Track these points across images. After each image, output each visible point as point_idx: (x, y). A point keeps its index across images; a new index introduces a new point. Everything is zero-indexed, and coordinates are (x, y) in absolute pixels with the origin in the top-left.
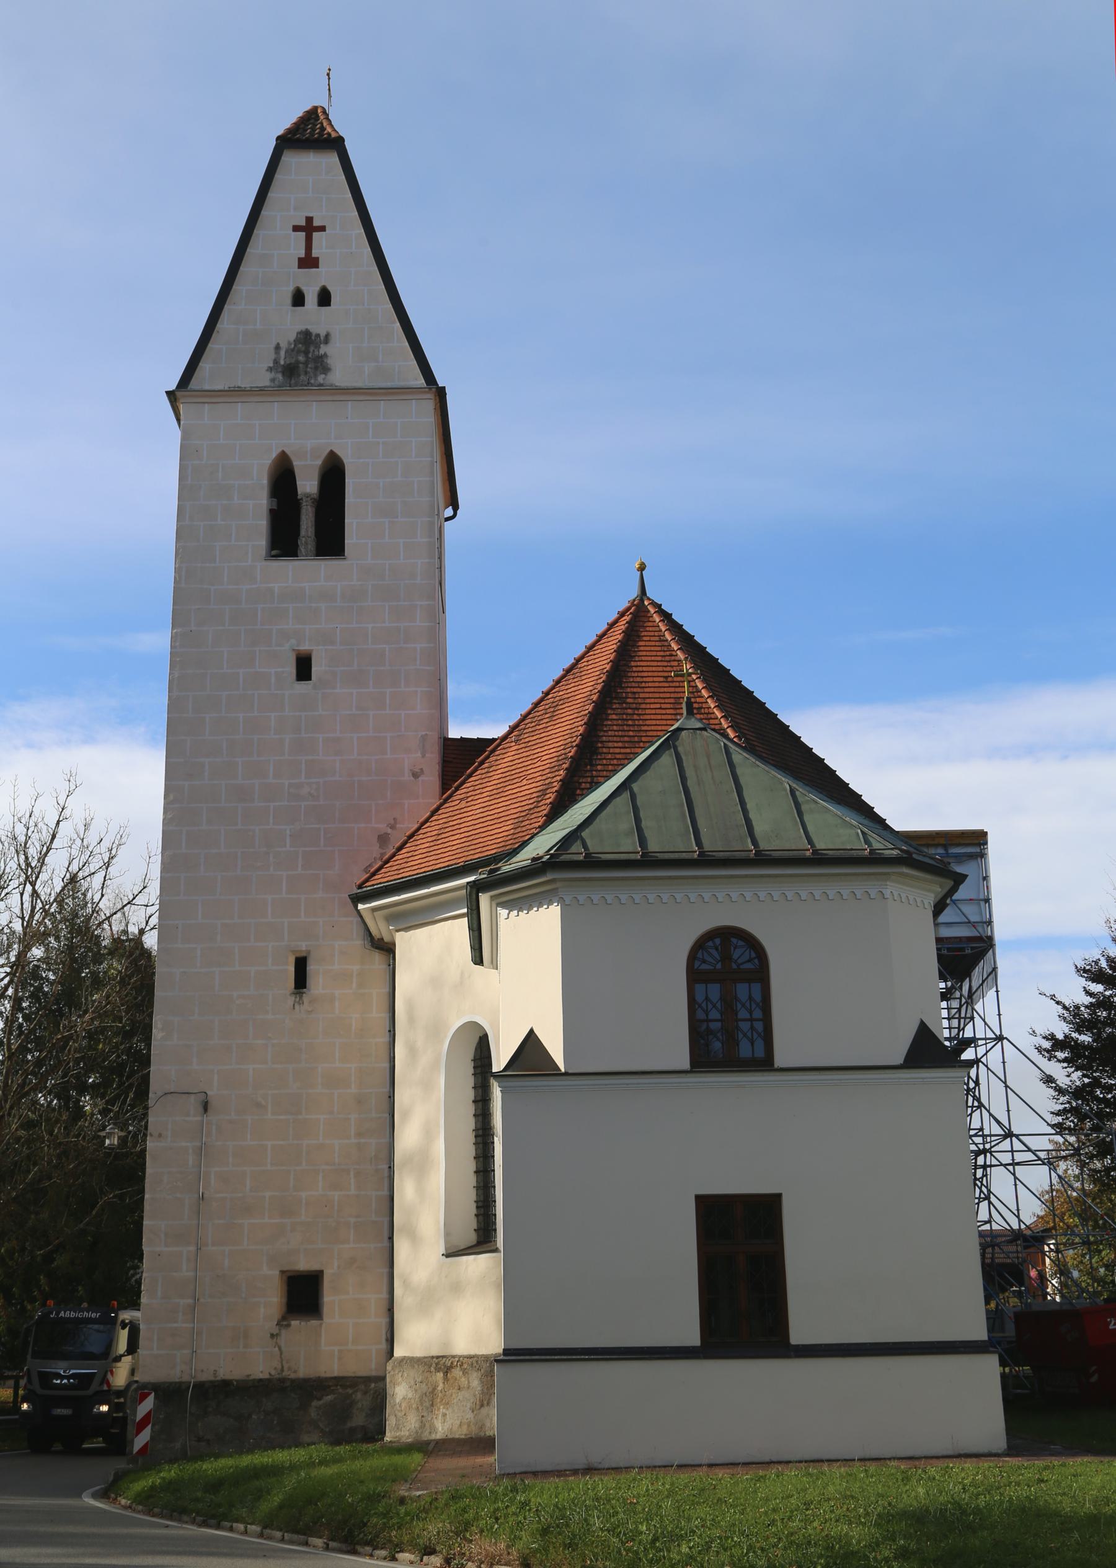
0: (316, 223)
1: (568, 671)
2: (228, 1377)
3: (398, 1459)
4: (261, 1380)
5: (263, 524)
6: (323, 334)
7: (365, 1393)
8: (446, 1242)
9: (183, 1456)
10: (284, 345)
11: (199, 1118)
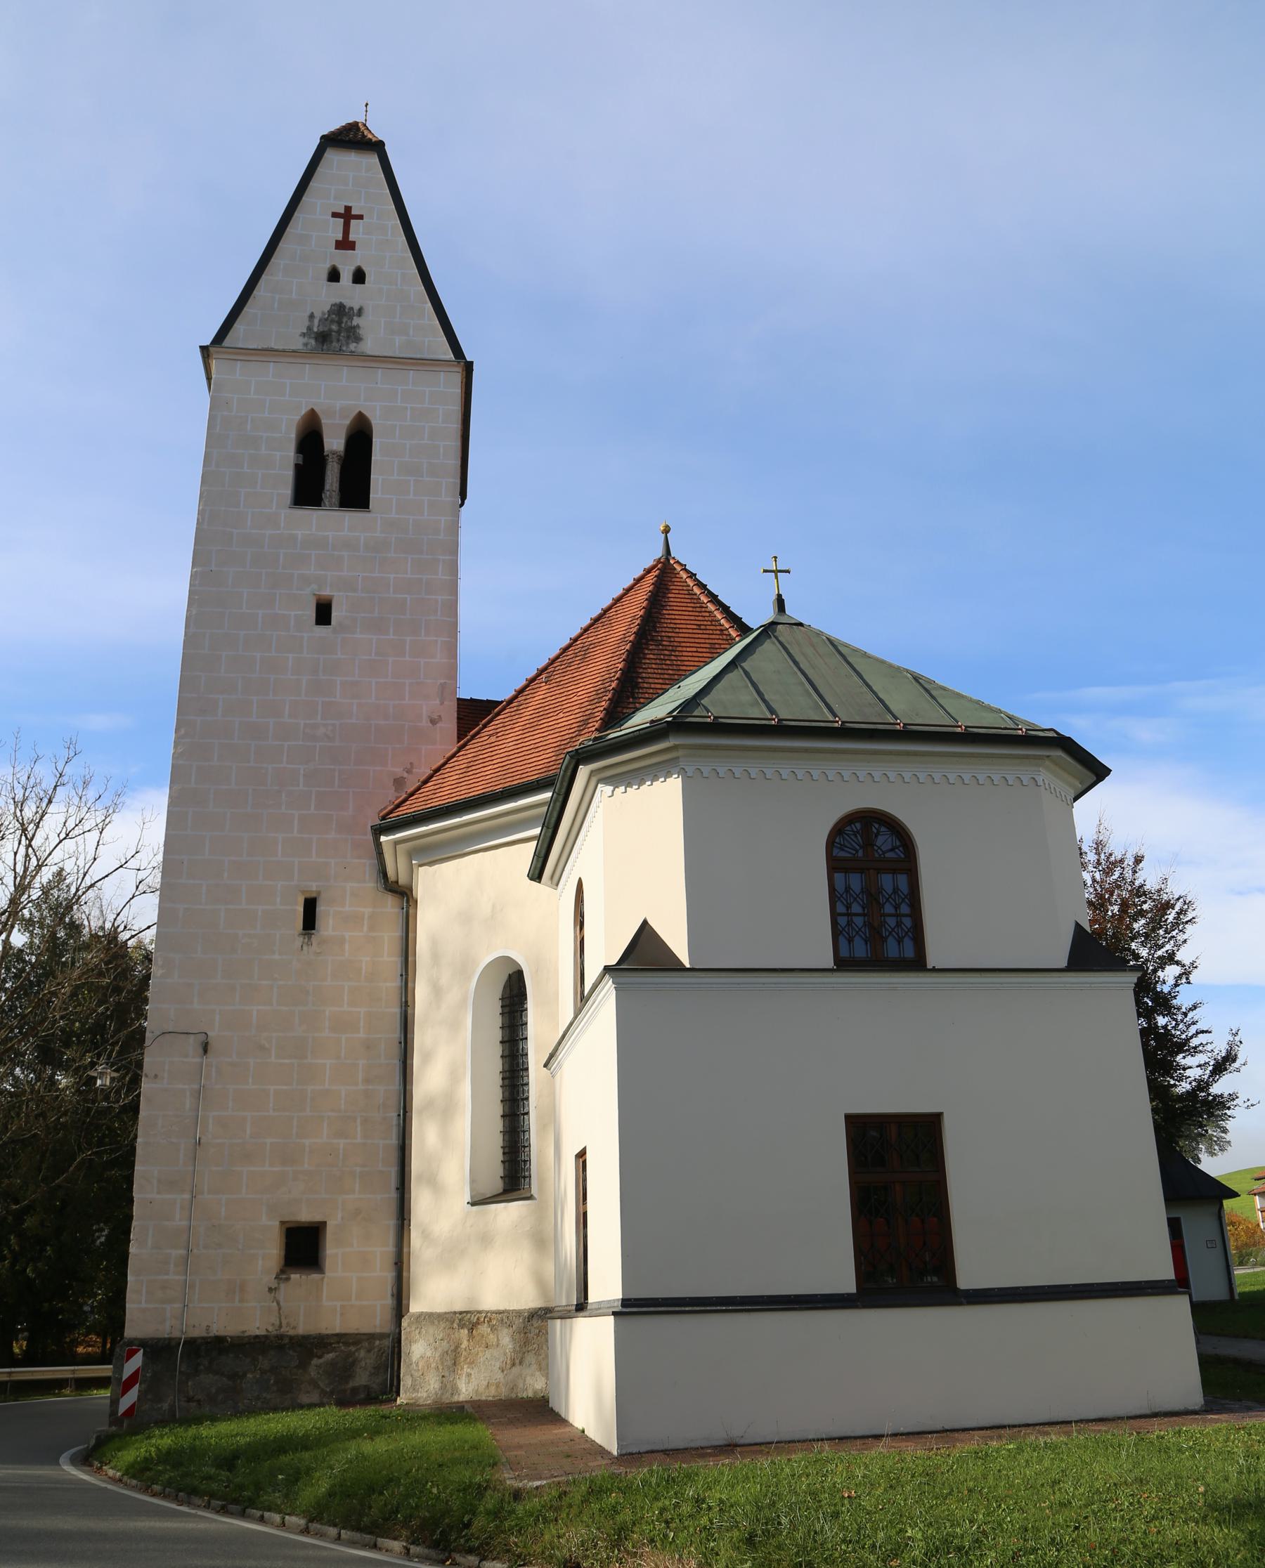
0: (353, 212)
1: (596, 620)
2: (222, 1333)
3: (480, 1432)
4: (257, 1337)
5: (288, 475)
6: (356, 308)
7: (369, 1351)
8: (472, 1190)
9: (169, 1420)
10: (318, 315)
11: (198, 1060)
